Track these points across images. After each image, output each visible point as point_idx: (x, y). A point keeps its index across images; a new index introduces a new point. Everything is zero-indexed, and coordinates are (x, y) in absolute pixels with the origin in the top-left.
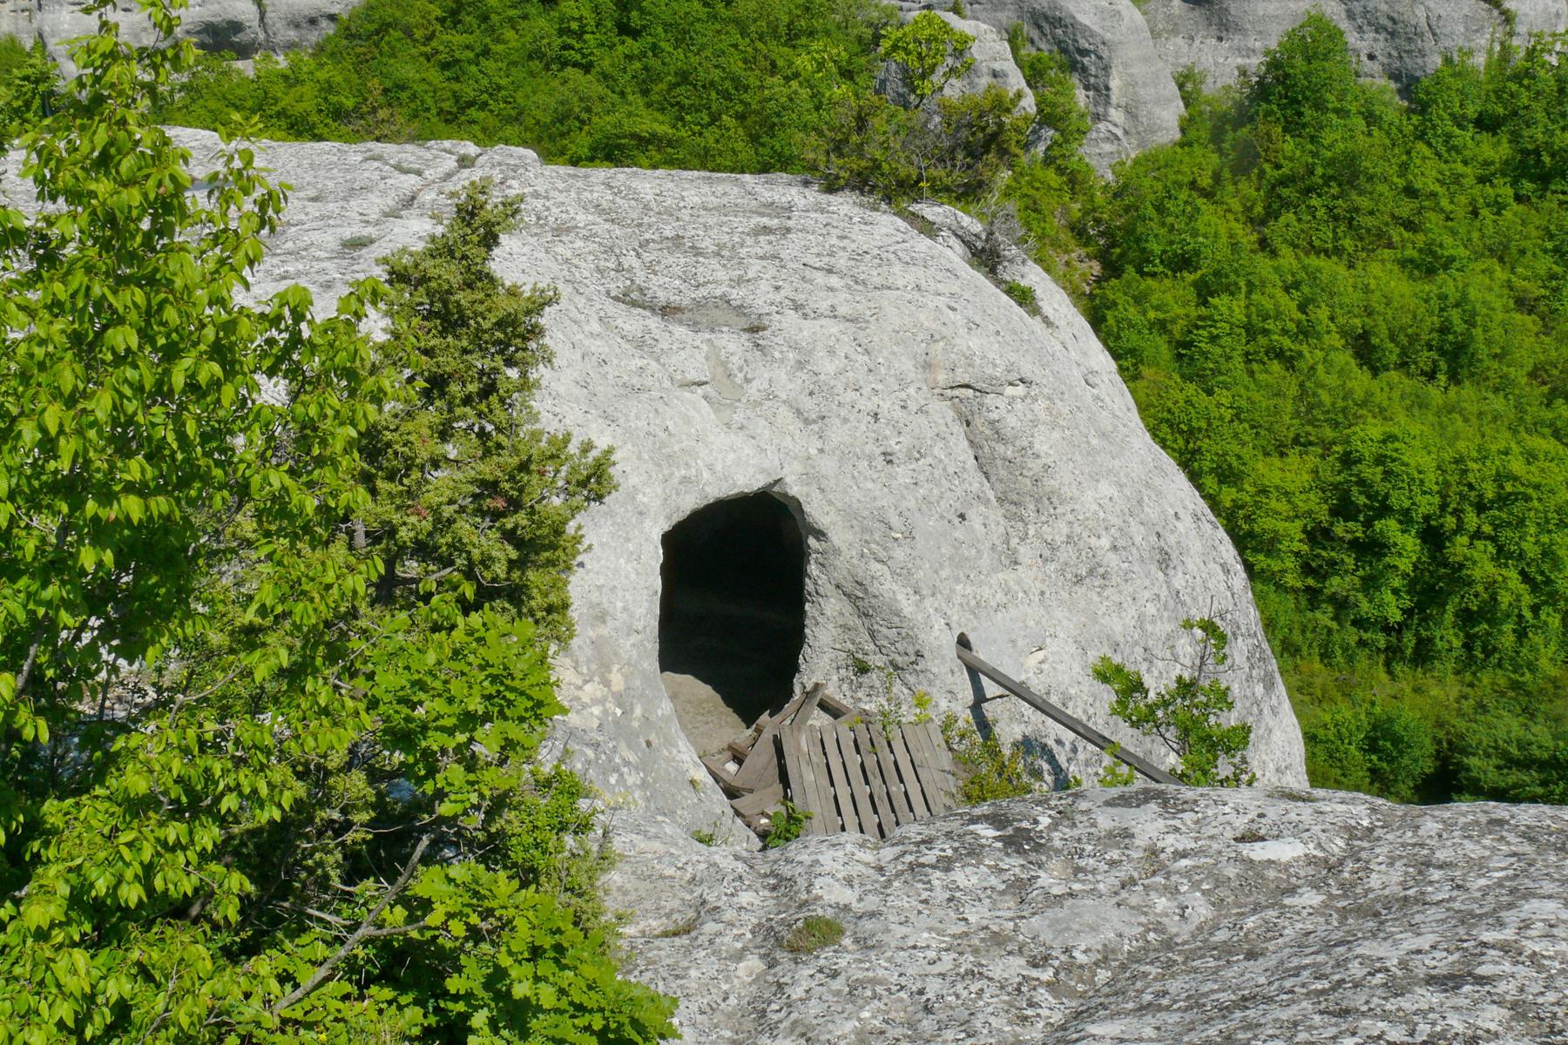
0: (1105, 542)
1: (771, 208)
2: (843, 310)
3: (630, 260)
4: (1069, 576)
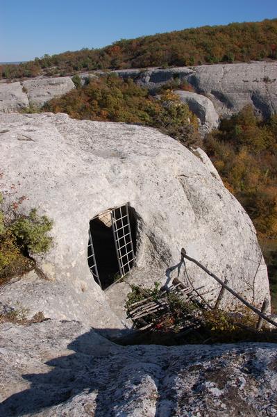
0: (222, 220)
1: (130, 130)
2: (149, 153)
3: (89, 140)
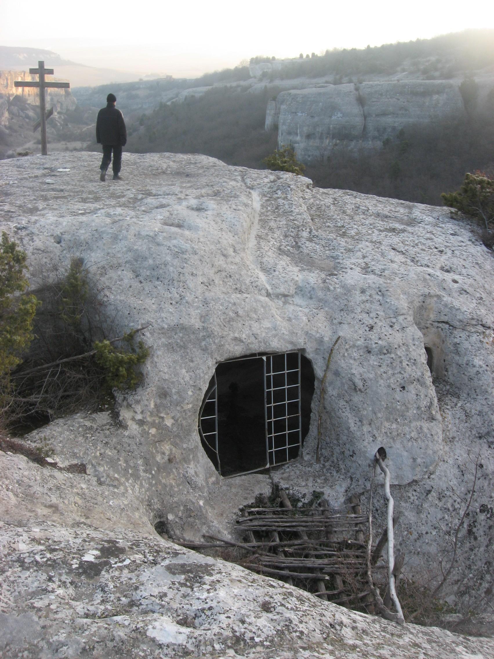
4: (474, 433)
